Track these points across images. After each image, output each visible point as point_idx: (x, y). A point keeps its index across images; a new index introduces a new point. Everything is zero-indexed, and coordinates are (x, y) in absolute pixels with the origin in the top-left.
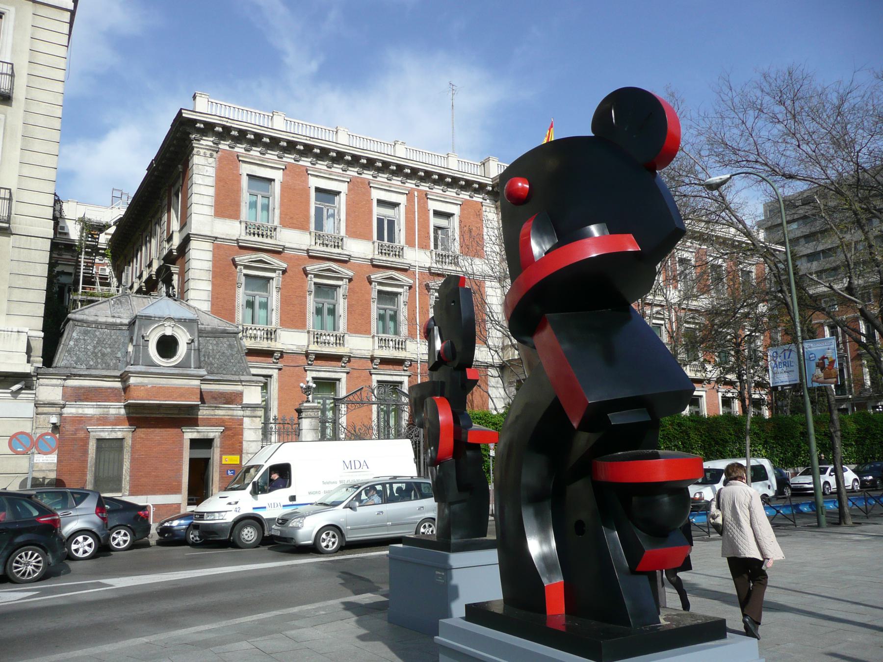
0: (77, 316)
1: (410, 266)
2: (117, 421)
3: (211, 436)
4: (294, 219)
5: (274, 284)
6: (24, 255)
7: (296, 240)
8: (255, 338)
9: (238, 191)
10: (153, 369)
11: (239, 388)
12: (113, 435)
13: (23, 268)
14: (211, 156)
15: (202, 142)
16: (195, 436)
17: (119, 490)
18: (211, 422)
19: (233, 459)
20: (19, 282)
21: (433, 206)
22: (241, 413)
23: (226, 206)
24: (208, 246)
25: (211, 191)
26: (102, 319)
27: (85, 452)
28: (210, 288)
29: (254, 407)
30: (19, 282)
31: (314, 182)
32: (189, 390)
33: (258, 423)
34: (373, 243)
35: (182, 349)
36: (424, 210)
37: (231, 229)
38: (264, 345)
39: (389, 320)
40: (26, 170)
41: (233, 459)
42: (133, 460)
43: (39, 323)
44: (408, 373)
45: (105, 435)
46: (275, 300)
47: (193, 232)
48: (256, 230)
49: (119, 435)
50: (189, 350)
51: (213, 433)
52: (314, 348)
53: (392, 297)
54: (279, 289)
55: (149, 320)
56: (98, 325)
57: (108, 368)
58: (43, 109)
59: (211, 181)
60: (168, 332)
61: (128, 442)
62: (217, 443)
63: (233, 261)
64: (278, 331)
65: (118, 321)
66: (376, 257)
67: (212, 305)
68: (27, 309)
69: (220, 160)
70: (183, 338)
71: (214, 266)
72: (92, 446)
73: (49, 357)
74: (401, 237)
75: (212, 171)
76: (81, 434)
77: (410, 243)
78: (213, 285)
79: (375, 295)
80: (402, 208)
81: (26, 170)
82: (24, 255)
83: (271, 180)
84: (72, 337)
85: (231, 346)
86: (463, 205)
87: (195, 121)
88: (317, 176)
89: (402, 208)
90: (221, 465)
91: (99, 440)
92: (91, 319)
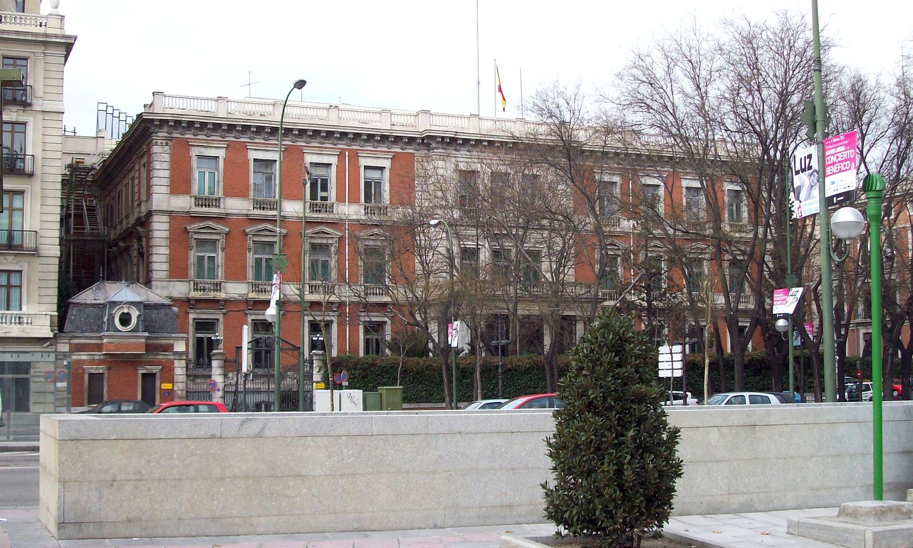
0: (75, 301)
1: (341, 220)
2: (100, 362)
3: (154, 371)
4: (236, 188)
5: (220, 245)
6: (45, 268)
7: (236, 206)
8: (204, 290)
9: (190, 170)
10: (118, 334)
11: (172, 342)
12: (98, 372)
13: (44, 276)
14: (167, 144)
15: (159, 134)
16: (144, 371)
17: (876, 534)
18: (151, 363)
19: (168, 386)
20: (44, 284)
21: (363, 162)
22: (172, 357)
23: (180, 183)
24: (165, 218)
25: (167, 174)
26: (89, 302)
27: (83, 381)
28: (168, 252)
29: (180, 354)
30: (44, 284)
31: (253, 155)
32: (136, 346)
33: (183, 363)
34: (305, 202)
35: (134, 321)
36: (355, 166)
37: (182, 203)
38: (211, 295)
39: (320, 270)
40: (45, 218)
41: (168, 386)
42: (109, 386)
43: (55, 307)
44: (336, 313)
45: (93, 371)
46: (220, 257)
47: (154, 208)
48: (201, 201)
49: (101, 371)
50: (138, 321)
51: (155, 369)
52: (252, 295)
53: (324, 248)
54: (223, 249)
55: (114, 304)
56: (87, 305)
57: (93, 331)
58: (50, 186)
59: (166, 166)
60: (126, 311)
61: (106, 375)
62: (158, 376)
63: (186, 228)
64: (223, 284)
65: (98, 302)
66: (309, 215)
67: (170, 265)
68: (48, 299)
69: (173, 148)
70: (135, 314)
71: (170, 234)
72: (86, 377)
73: (61, 328)
74: (332, 194)
75: (167, 157)
76: (80, 371)
77: (341, 199)
78: (171, 249)
79: (307, 247)
80: (334, 168)
81: (45, 218)
82: (45, 268)
83: (216, 158)
84: (72, 313)
85: (166, 314)
86: (395, 158)
87: (153, 120)
88: (255, 150)
89: (334, 168)
90: (161, 390)
91: (90, 374)
92: (83, 302)
